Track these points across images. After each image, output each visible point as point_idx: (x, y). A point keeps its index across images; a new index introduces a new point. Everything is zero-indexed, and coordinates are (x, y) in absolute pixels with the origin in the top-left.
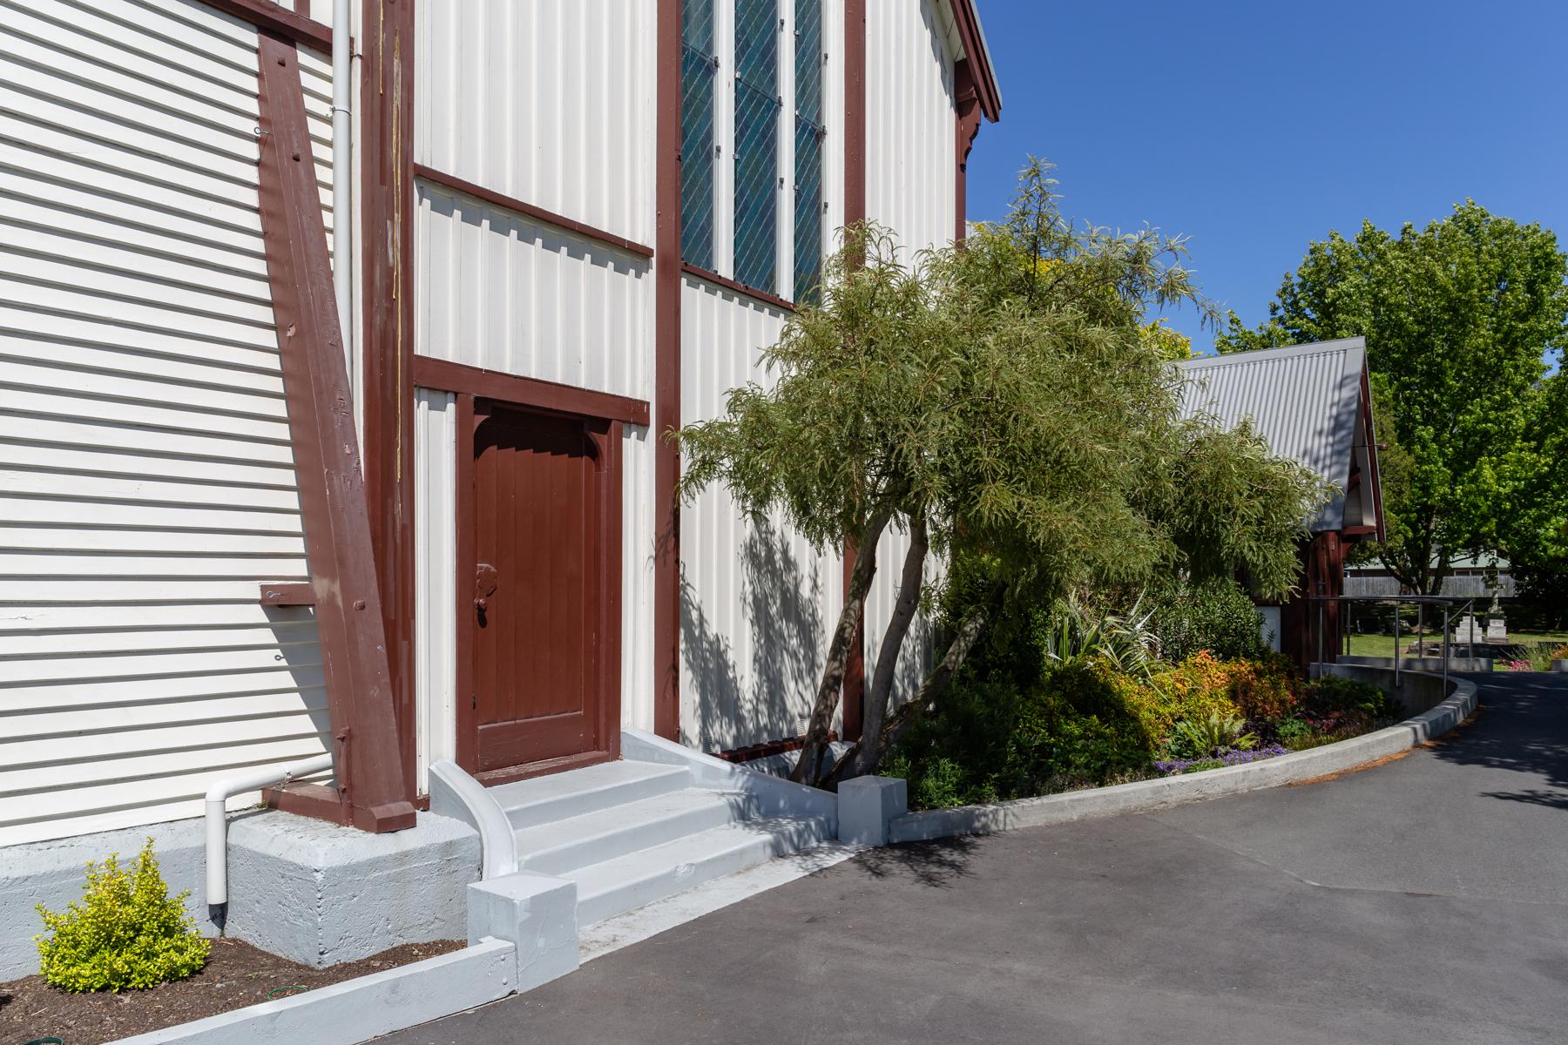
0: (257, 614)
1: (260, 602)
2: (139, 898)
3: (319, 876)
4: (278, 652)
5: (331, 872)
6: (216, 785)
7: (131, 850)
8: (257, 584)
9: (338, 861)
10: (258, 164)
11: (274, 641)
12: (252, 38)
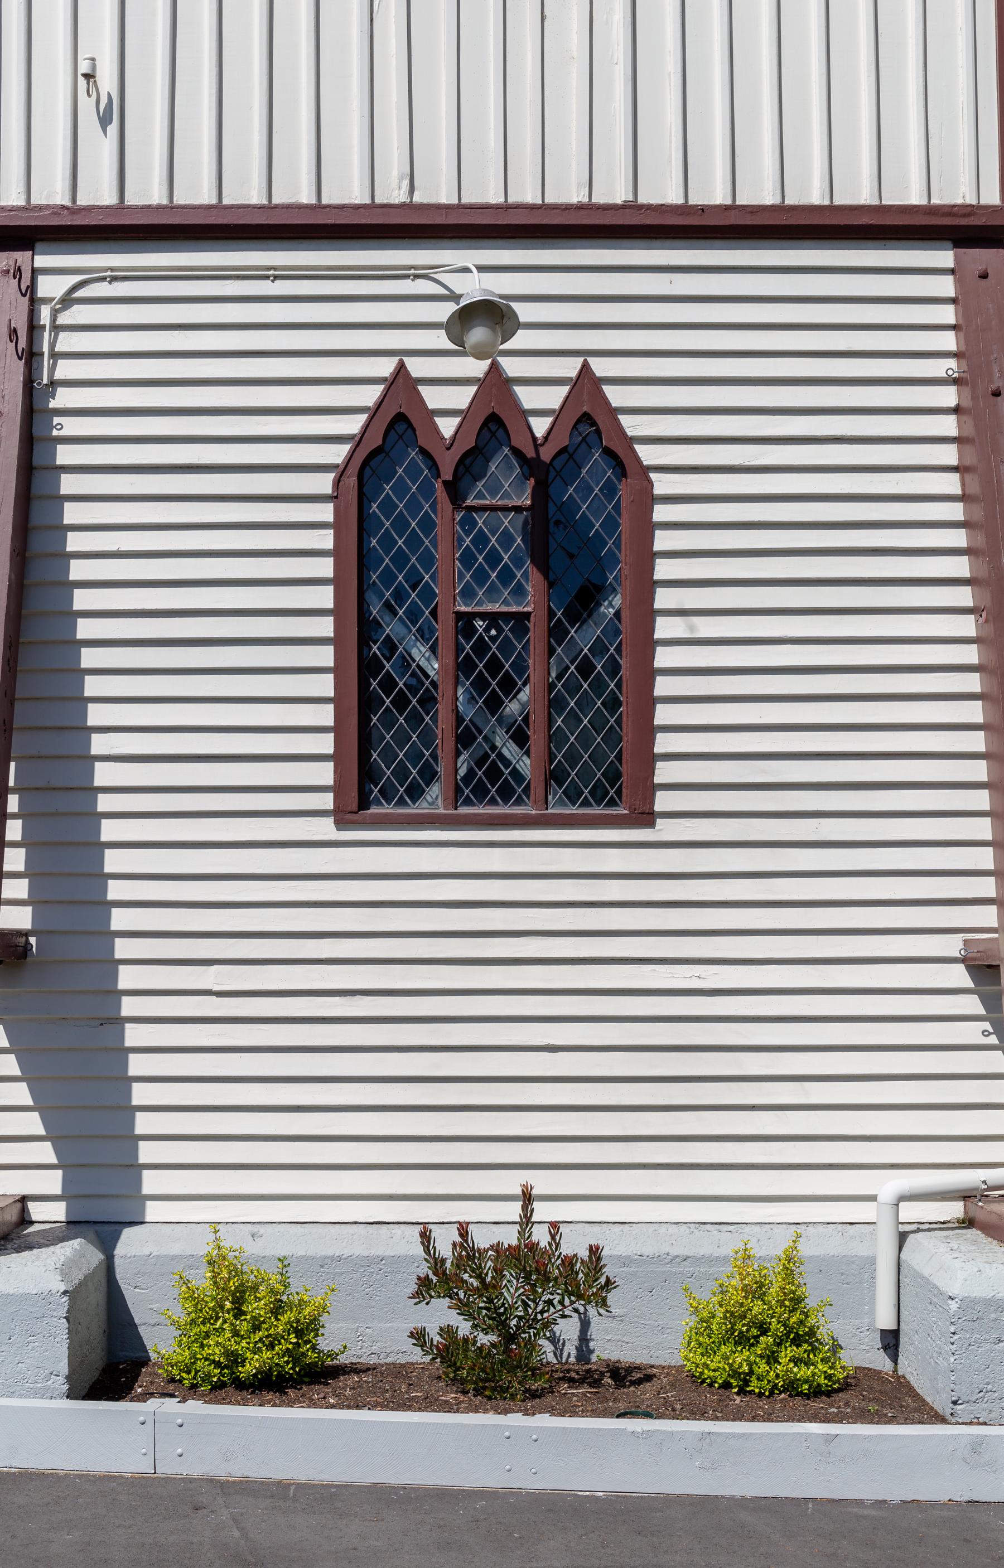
0: (959, 976)
1: (963, 960)
2: (773, 1293)
3: (953, 1305)
4: (987, 1026)
5: (968, 1303)
6: (889, 1185)
7: (770, 1248)
8: (960, 937)
9: (981, 1291)
10: (956, 410)
11: (981, 1011)
12: (945, 257)
